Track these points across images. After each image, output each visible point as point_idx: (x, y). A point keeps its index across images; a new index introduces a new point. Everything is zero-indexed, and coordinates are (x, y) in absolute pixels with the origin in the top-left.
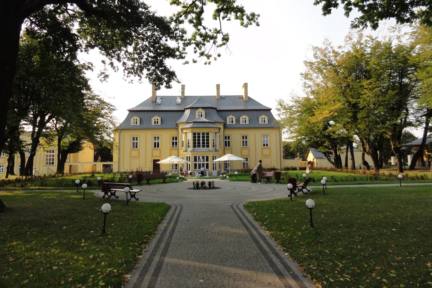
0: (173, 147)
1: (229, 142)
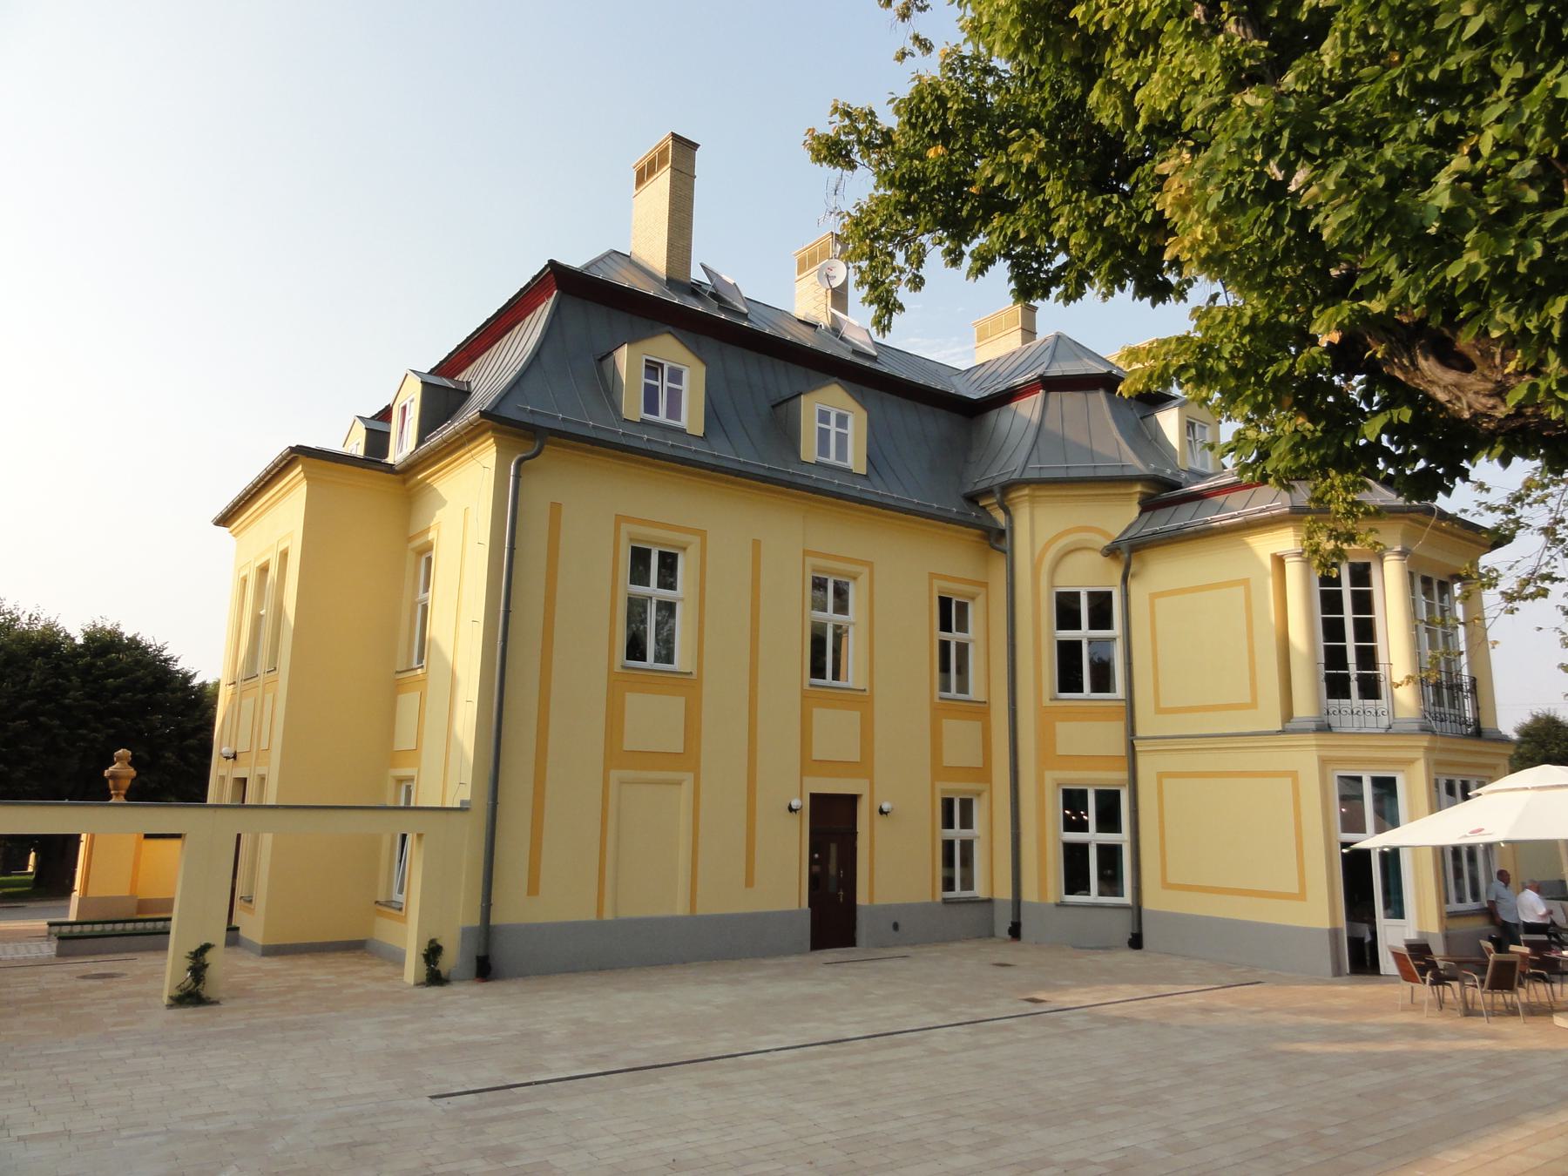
0: (945, 687)
1: (948, 823)
